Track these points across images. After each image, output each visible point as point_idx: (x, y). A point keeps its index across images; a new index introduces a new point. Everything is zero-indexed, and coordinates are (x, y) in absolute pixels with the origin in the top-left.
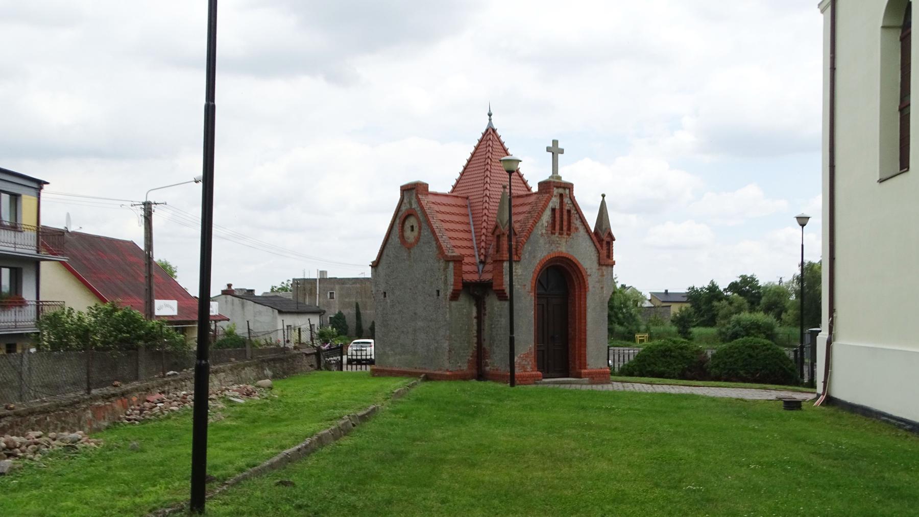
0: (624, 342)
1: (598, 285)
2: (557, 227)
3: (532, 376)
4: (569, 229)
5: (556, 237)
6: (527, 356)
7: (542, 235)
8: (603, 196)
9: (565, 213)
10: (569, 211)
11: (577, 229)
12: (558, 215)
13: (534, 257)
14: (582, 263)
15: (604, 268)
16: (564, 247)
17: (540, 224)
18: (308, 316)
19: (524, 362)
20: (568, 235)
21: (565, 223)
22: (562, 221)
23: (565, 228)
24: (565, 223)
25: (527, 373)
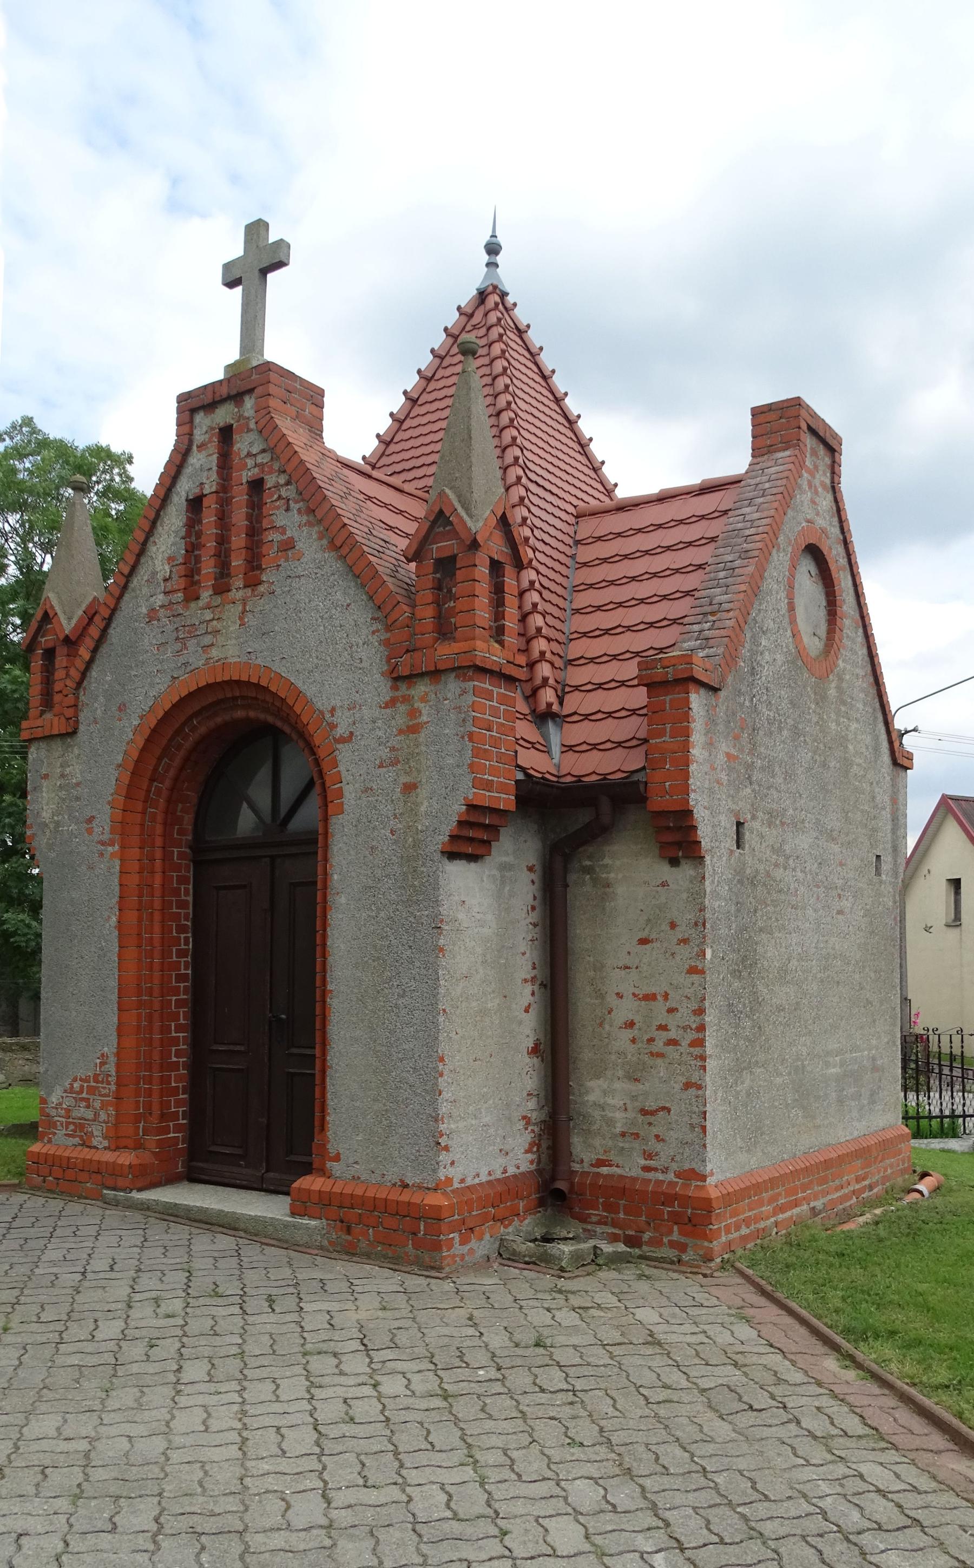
0: (347, 1258)
1: (389, 779)
2: (208, 567)
3: (97, 1170)
4: (254, 564)
5: (197, 613)
6: (93, 1084)
7: (152, 615)
8: (915, 730)
9: (240, 497)
10: (257, 486)
11: (288, 546)
12: (209, 518)
13: (122, 708)
14: (309, 690)
15: (422, 688)
16: (236, 641)
17: (143, 574)
18: (914, 935)
19: (81, 1112)
20: (252, 583)
21: (238, 541)
22: (222, 541)
23: (237, 562)
24: (238, 541)
25: (87, 1154)
